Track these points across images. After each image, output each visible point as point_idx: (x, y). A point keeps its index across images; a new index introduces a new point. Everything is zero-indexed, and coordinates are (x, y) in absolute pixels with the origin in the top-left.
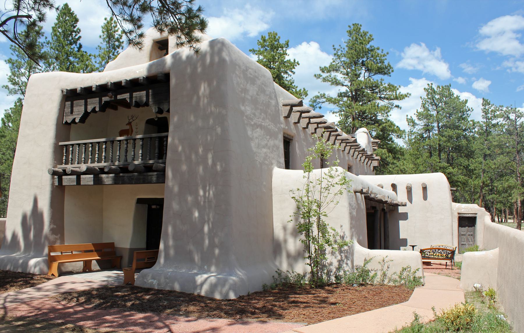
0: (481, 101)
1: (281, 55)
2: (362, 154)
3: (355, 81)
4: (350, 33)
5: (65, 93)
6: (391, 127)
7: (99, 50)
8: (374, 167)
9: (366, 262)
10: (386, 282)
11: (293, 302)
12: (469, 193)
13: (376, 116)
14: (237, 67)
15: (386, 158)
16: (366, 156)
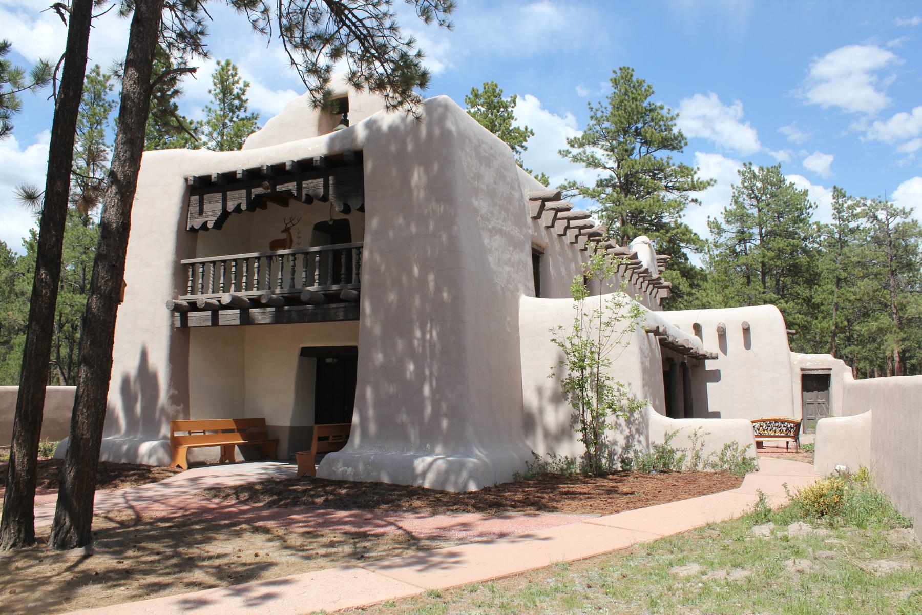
0: (830, 194)
1: (504, 120)
2: (644, 277)
3: (626, 160)
4: (615, 82)
5: (191, 183)
6: (686, 235)
7: (208, 113)
8: (662, 299)
9: (668, 437)
10: (700, 467)
11: (567, 493)
12: (812, 343)
13: (659, 217)
14: (467, 141)
15: (679, 284)
16: (649, 281)
